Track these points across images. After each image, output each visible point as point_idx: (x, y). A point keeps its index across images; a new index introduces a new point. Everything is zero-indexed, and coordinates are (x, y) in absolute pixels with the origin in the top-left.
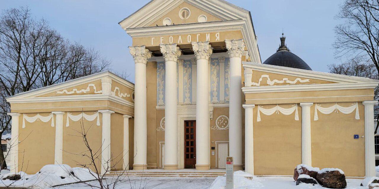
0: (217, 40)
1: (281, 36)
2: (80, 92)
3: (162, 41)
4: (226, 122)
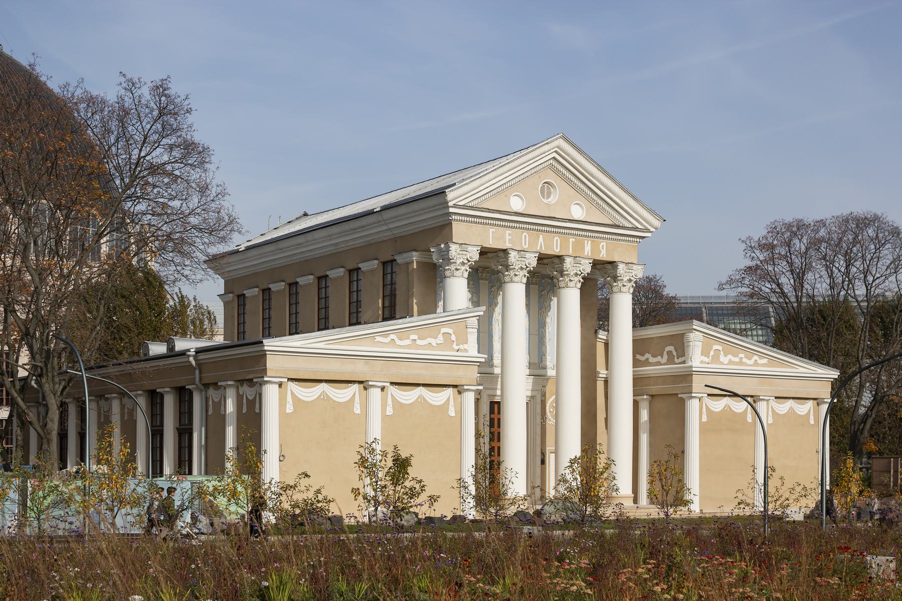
0: (601, 256)
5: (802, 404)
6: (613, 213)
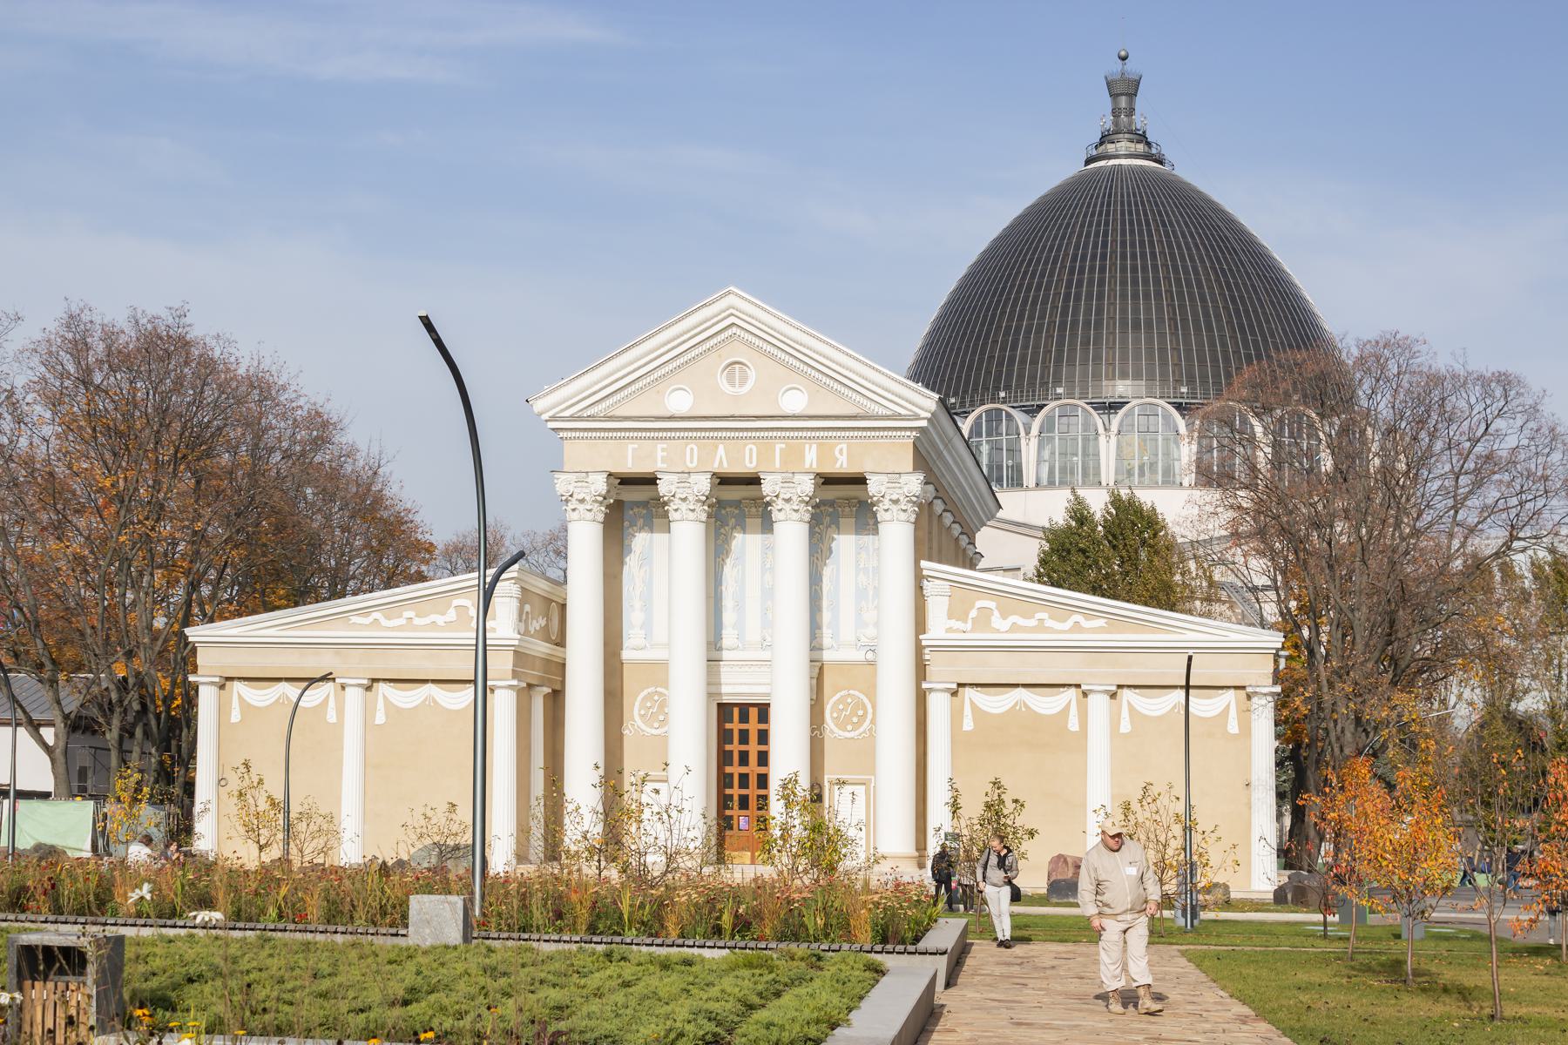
0: (838, 465)
1: (1116, 67)
2: (427, 620)
3: (662, 457)
4: (860, 713)
5: (1209, 697)
6: (858, 398)
